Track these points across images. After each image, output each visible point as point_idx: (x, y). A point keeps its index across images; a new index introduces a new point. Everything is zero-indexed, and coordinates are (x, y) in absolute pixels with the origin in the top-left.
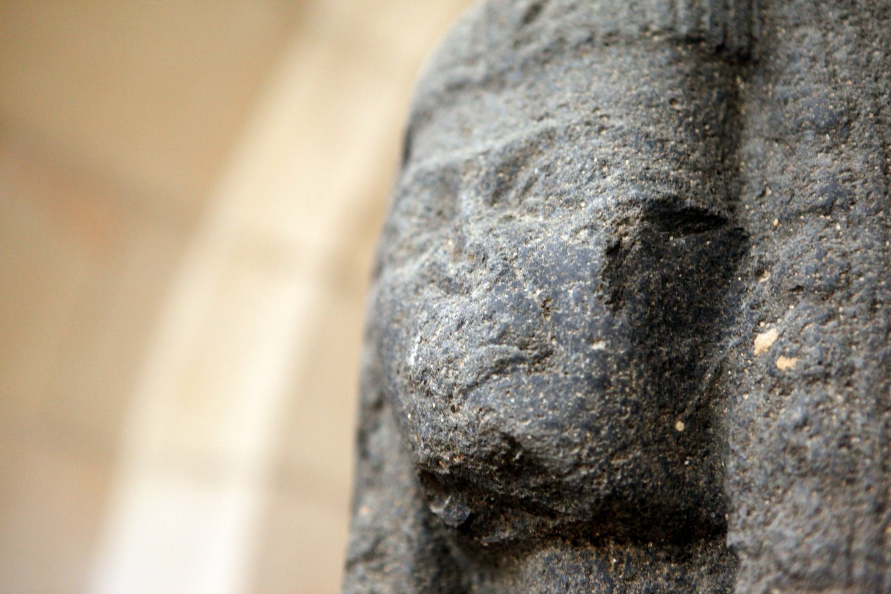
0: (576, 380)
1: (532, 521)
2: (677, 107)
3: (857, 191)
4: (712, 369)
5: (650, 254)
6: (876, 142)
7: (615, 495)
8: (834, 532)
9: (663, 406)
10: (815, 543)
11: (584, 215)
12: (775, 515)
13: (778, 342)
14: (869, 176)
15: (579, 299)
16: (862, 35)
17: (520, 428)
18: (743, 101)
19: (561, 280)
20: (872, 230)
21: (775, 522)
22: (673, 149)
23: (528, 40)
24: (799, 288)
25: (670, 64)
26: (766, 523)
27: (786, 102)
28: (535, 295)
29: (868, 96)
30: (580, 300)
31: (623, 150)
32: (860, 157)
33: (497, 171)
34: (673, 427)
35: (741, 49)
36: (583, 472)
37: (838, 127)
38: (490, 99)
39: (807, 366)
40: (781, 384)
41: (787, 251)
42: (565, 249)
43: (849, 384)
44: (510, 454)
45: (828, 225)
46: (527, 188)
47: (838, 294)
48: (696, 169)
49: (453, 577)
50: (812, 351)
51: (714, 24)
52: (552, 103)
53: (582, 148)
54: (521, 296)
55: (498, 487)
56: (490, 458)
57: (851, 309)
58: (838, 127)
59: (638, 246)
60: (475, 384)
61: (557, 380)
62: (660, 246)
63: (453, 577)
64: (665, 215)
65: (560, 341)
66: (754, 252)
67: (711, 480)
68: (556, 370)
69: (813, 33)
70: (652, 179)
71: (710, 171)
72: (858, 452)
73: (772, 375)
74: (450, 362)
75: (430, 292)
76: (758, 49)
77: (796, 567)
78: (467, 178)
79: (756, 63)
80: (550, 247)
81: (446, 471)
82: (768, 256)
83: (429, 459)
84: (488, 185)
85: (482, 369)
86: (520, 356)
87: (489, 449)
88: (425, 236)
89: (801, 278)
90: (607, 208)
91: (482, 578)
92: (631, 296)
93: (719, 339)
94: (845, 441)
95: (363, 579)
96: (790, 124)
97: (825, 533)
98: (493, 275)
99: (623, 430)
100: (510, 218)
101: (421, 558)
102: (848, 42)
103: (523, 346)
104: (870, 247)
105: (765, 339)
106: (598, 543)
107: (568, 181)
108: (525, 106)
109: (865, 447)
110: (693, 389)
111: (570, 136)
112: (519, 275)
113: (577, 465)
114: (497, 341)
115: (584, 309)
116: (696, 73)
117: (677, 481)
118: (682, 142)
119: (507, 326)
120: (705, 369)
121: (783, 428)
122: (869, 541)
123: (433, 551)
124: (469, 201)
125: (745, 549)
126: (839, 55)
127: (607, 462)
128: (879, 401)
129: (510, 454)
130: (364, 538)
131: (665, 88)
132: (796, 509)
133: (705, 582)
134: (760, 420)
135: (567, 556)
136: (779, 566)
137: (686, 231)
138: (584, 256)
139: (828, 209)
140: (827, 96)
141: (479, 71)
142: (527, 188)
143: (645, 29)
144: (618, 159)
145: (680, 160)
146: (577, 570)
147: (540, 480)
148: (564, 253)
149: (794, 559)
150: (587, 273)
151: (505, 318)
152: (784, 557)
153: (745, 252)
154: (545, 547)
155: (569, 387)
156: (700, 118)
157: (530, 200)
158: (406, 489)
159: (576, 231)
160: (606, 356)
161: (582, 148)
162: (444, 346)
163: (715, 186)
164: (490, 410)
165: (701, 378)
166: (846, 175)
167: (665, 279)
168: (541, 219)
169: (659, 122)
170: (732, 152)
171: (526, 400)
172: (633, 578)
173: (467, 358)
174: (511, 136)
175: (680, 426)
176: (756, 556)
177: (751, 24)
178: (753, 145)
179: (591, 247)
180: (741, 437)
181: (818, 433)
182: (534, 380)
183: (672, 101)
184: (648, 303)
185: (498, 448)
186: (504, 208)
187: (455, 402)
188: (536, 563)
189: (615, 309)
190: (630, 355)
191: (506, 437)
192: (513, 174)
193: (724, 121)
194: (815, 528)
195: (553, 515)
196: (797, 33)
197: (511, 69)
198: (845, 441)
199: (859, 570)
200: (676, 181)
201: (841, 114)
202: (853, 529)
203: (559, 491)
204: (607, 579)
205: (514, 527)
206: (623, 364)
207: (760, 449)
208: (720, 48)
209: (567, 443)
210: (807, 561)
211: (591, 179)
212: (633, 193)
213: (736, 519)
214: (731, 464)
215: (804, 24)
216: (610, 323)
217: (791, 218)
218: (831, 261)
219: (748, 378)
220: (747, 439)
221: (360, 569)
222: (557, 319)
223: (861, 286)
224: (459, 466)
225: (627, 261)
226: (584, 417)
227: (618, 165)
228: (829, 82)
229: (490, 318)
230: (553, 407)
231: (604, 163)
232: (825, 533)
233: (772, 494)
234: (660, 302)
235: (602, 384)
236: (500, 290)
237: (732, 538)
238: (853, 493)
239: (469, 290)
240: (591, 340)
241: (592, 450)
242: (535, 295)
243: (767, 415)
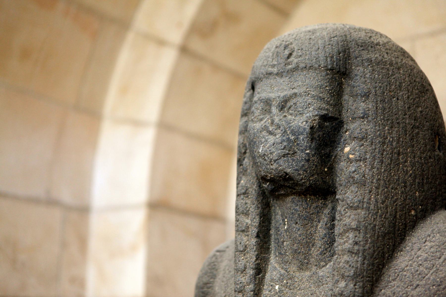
0: (302, 159)
1: (289, 190)
2: (327, 88)
3: (370, 113)
4: (334, 156)
5: (320, 128)
6: (375, 101)
7: (311, 186)
8: (360, 197)
9: (322, 165)
10: (356, 200)
11: (304, 118)
12: (347, 192)
13: (350, 151)
14: (373, 110)
15: (303, 140)
16: (373, 70)
17: (288, 171)
18: (343, 85)
19: (299, 135)
20: (373, 124)
21: (347, 194)
22: (326, 101)
23: (289, 64)
24: (355, 137)
25: (326, 76)
26: (345, 194)
27: (354, 87)
28: (292, 138)
29: (373, 88)
30: (303, 140)
31: (314, 101)
32: (371, 104)
33: (282, 103)
34: (324, 170)
35: (343, 72)
36: (303, 181)
37: (366, 96)
38: (278, 79)
39: (356, 158)
40: (350, 161)
41: (353, 127)
42: (300, 127)
43: (365, 162)
44: (286, 176)
45: (363, 122)
46: (290, 108)
47: (364, 140)
48: (331, 105)
49: (266, 199)
50: (358, 154)
51: (337, 65)
52: (296, 84)
53: (304, 99)
54: (289, 138)
55: (282, 183)
56: (281, 177)
57: (367, 144)
58: (366, 96)
59: (317, 126)
60: (277, 160)
61: (297, 160)
62: (323, 125)
63: (266, 199)
64: (324, 118)
65: (298, 150)
66: (345, 126)
67: (333, 181)
68: (297, 157)
69: (361, 69)
70: (321, 109)
71: (335, 106)
72: (367, 179)
73: (348, 159)
74: (271, 153)
75: (264, 133)
76: (348, 72)
77: (351, 205)
78: (274, 103)
79: (347, 75)
80: (296, 126)
81: (269, 178)
82: (348, 128)
83: (265, 175)
84: (279, 106)
85: (279, 156)
86: (289, 153)
87: (280, 175)
88: (262, 117)
89: (356, 135)
90: (310, 117)
91: (273, 200)
92: (315, 139)
93: (336, 148)
94: (364, 176)
95: (243, 199)
96: (355, 94)
97: (358, 197)
98: (282, 132)
99: (313, 171)
100: (285, 116)
101: (258, 195)
102: (369, 72)
103: (289, 151)
104: (372, 128)
105: (347, 149)
106: (305, 196)
107: (300, 108)
108: (288, 84)
109: (368, 178)
110: (329, 161)
111: (301, 95)
112: (288, 132)
113: (302, 179)
114: (283, 149)
115: (304, 142)
116: (332, 78)
117: (325, 182)
118: (328, 98)
119: (285, 146)
120: (332, 156)
121: (350, 172)
122: (367, 199)
123: (261, 193)
124: (274, 110)
125: (340, 199)
126: (367, 76)
127: (309, 178)
128: (372, 167)
129: (286, 176)
130: (243, 189)
131: (325, 83)
132: (352, 191)
133: (330, 204)
134: (345, 169)
135: (297, 198)
136: (348, 204)
137: (329, 122)
138: (305, 129)
139: (363, 118)
140: (364, 87)
141: (275, 70)
142: (290, 108)
143: (320, 66)
144: (313, 103)
145: (328, 103)
146: (300, 201)
147: (292, 182)
148: (300, 128)
149: (351, 203)
150: (305, 134)
151: (285, 144)
152: (349, 202)
153: (343, 126)
154: (292, 196)
155: (300, 161)
156: (333, 91)
157: (290, 111)
158: (254, 177)
159: (303, 122)
160: (309, 154)
161: (304, 99)
162: (270, 149)
163: (336, 109)
164: (281, 166)
165: (331, 158)
166: (367, 109)
167: (324, 134)
168: (293, 117)
169: (323, 93)
170: (340, 99)
171: (290, 164)
172: (313, 203)
173: (276, 153)
174: (285, 93)
175: (326, 170)
176: (343, 201)
177: (346, 65)
178: (346, 97)
179: (306, 127)
180: (340, 173)
181: (358, 174)
182: (292, 159)
183: (326, 87)
184: (319, 140)
185: (283, 175)
186: (283, 113)
187: (272, 163)
188: (289, 199)
189: (312, 142)
190: (315, 154)
191: (285, 172)
192: (286, 103)
193: (339, 91)
194: (356, 196)
195: (295, 189)
196: (358, 68)
197: (284, 72)
198: (364, 176)
199: (365, 206)
200: (327, 109)
201: (367, 92)
202: (364, 197)
203: (297, 184)
204: (307, 204)
205: (284, 191)
206: (313, 156)
207: (344, 176)
208: (338, 72)
209: (300, 174)
210: (354, 203)
211: (306, 108)
212: (316, 113)
213: (339, 192)
214: (338, 179)
215: (359, 66)
216: (310, 146)
217: (354, 119)
218: (363, 132)
219: (343, 159)
220: (342, 173)
221: (242, 196)
222: (298, 144)
223: (370, 138)
224: (272, 178)
225: (315, 130)
226: (304, 168)
227: (313, 105)
228: (365, 84)
229: (281, 143)
230: (296, 166)
231: (309, 104)
232: (358, 197)
233: (347, 187)
234: (322, 140)
235: (308, 161)
236: (284, 136)
237: (337, 197)
238: (365, 188)
239: (275, 135)
240: (306, 150)
241: (305, 176)
242: (292, 138)
243: (346, 168)
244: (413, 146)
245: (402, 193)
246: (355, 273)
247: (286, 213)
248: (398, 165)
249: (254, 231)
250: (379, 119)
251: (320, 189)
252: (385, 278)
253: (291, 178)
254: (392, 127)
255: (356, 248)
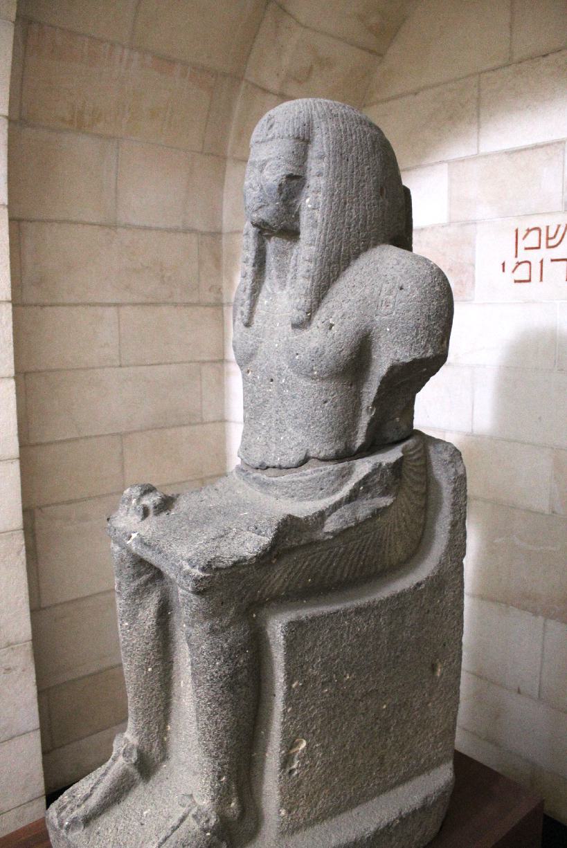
64: (290, 177)
145: (294, 165)
235: (278, 210)
244: (358, 196)
245: (347, 233)
246: (306, 292)
247: (272, 245)
248: (345, 211)
249: (251, 261)
250: (330, 176)
251: (291, 233)
252: (329, 295)
253: (267, 224)
254: (341, 182)
255: (308, 274)
